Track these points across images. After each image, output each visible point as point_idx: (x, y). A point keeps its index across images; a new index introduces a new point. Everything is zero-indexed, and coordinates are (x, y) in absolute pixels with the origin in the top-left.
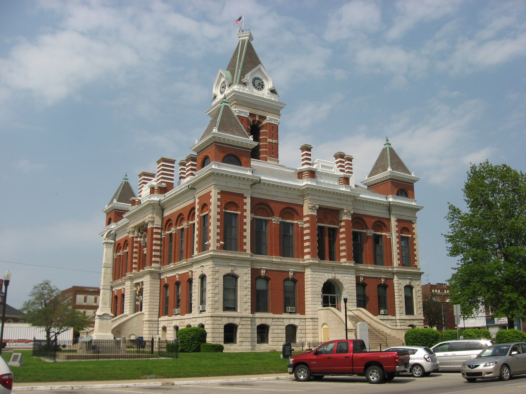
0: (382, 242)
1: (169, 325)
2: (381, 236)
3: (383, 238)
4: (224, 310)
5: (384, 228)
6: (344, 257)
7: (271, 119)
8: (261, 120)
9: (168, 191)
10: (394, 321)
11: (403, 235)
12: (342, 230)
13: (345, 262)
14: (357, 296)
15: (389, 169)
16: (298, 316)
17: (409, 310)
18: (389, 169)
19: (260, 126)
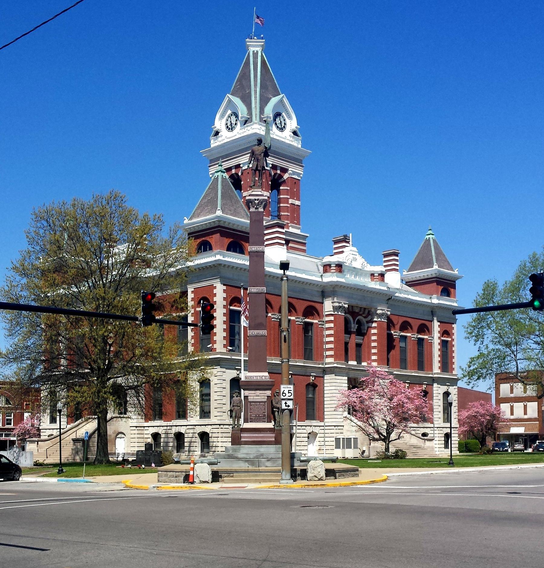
0: (313, 333)
1: (188, 431)
2: (312, 324)
3: (314, 326)
4: (201, 418)
5: (316, 314)
6: (374, 361)
7: (294, 173)
8: (282, 174)
9: (282, 286)
10: (432, 429)
11: (231, 308)
12: (374, 331)
13: (376, 367)
14: (209, 400)
15: (436, 267)
16: (314, 423)
17: (447, 418)
18: (436, 267)
19: (280, 181)
